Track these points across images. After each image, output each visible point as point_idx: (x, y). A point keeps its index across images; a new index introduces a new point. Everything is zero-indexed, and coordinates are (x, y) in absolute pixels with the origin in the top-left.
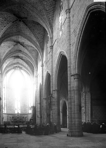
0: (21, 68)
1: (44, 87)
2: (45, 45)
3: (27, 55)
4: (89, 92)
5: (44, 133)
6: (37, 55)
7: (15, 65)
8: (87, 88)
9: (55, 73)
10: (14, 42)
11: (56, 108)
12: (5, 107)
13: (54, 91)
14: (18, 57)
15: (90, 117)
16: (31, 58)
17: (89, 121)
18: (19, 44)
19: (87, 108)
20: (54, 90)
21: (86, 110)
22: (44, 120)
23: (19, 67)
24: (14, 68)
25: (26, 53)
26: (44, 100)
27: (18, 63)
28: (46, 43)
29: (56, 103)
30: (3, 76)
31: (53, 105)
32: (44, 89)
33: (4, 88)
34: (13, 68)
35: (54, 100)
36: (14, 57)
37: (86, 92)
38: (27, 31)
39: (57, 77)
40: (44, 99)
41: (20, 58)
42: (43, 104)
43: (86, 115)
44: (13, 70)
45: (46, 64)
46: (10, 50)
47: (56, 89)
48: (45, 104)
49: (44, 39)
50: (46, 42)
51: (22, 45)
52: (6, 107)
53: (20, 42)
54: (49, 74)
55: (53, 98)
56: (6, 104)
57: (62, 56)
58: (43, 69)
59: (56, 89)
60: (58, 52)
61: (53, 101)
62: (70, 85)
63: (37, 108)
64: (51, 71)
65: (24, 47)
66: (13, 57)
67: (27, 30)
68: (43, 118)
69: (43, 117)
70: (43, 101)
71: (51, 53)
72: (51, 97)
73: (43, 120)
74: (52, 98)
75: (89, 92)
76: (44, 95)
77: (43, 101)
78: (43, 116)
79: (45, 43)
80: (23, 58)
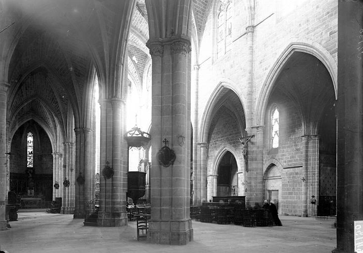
3: (143, 35)
4: (315, 136)
5: (108, 224)
8: (311, 127)
13: (255, 129)
15: (316, 189)
17: (313, 197)
19: (310, 169)
21: (307, 174)
22: (198, 193)
25: (141, 32)
26: (199, 146)
28: (214, 17)
31: (252, 160)
37: (308, 136)
39: (266, 98)
43: (306, 185)
48: (202, 156)
49: (206, 5)
50: (214, 14)
57: (292, 52)
61: (251, 151)
64: (249, 83)
68: (196, 189)
69: (196, 186)
70: (196, 150)
73: (196, 193)
74: (249, 143)
75: (315, 136)
77: (196, 150)
78: (196, 183)
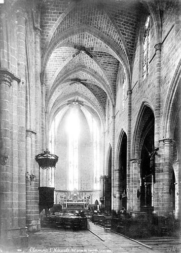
0: (81, 103)
1: (115, 156)
2: (138, 48)
6: (115, 74)
7: (71, 97)
9: (167, 102)
10: (75, 48)
11: (166, 177)
12: (52, 178)
14: (77, 80)
16: (104, 81)
18: (83, 52)
20: (162, 139)
23: (77, 101)
24: (69, 103)
27: (77, 93)
29: (166, 168)
30: (47, 59)
31: (159, 172)
32: (132, 141)
33: (51, 142)
34: (68, 104)
35: (161, 161)
36: (72, 80)
38: (101, 20)
40: (116, 170)
41: (82, 83)
42: (129, 172)
44: (67, 107)
45: (139, 87)
46: (66, 67)
47: (168, 137)
49: (135, 35)
50: (140, 40)
51: (89, 54)
52: (53, 177)
53: (86, 47)
54: (125, 133)
55: (159, 156)
56: (55, 173)
58: (130, 98)
59: (168, 137)
60: (120, 131)
62: (129, 176)
63: (113, 179)
65: (91, 57)
66: (68, 80)
67: (102, 17)
71: (156, 60)
72: (154, 155)
74: (156, 156)
76: (131, 152)
79: (139, 42)
80: (87, 82)
